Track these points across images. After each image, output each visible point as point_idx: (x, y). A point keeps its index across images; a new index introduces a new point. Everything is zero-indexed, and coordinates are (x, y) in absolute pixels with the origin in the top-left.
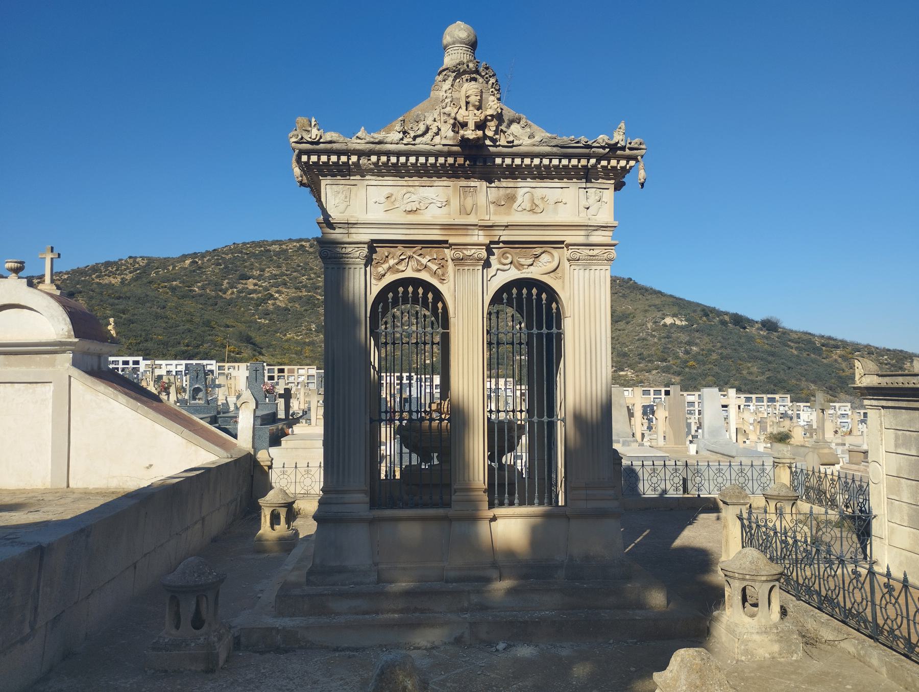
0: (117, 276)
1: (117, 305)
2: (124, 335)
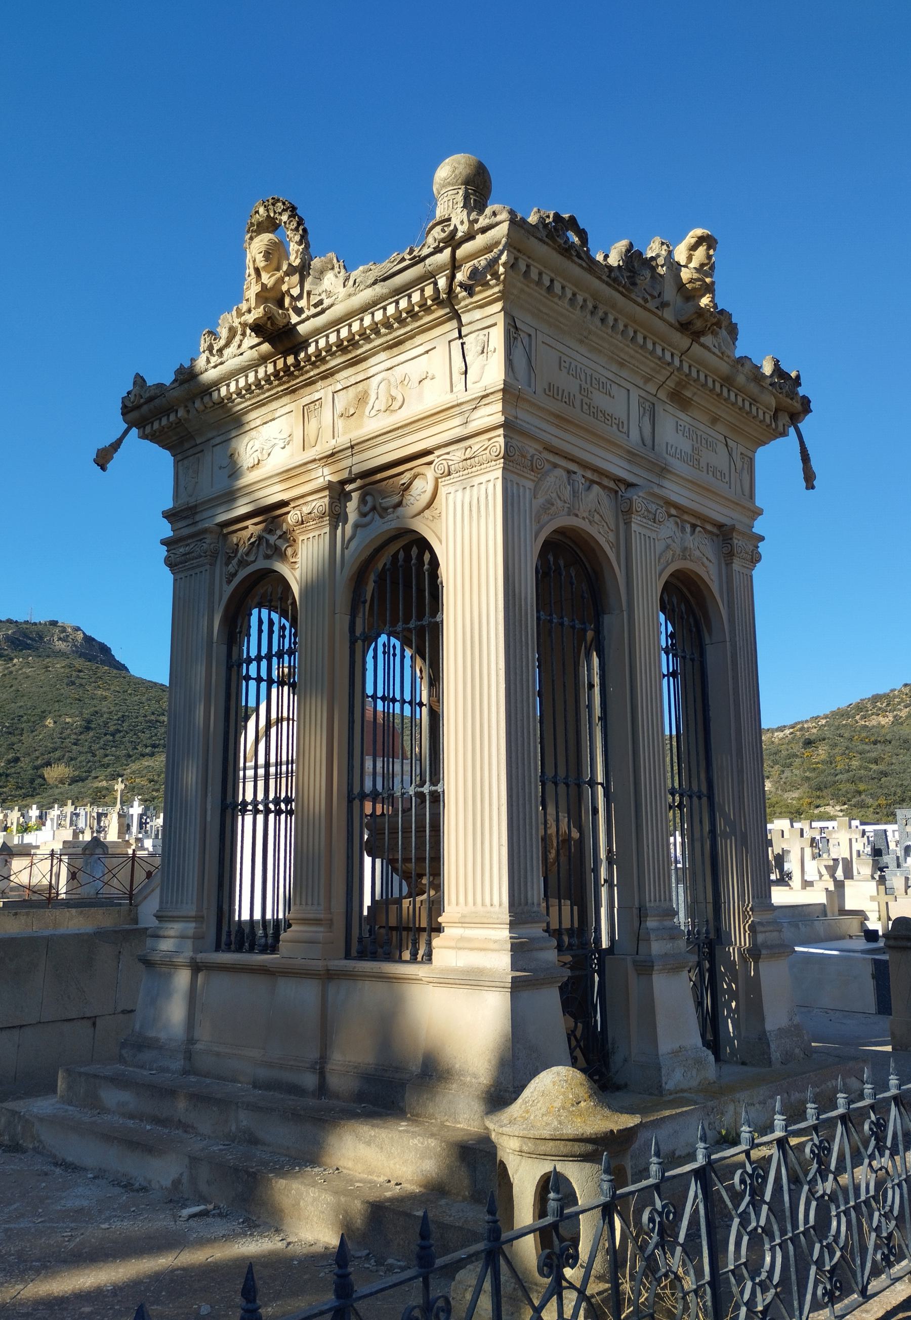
0: (887, 713)
1: (869, 752)
2: (871, 794)
